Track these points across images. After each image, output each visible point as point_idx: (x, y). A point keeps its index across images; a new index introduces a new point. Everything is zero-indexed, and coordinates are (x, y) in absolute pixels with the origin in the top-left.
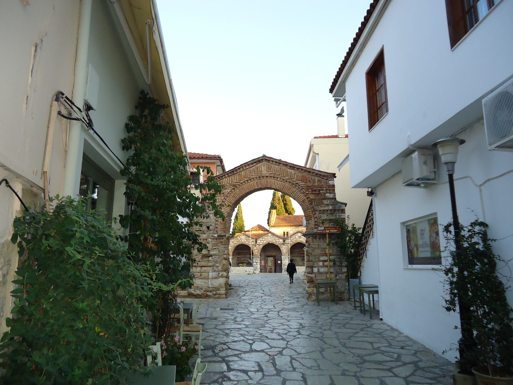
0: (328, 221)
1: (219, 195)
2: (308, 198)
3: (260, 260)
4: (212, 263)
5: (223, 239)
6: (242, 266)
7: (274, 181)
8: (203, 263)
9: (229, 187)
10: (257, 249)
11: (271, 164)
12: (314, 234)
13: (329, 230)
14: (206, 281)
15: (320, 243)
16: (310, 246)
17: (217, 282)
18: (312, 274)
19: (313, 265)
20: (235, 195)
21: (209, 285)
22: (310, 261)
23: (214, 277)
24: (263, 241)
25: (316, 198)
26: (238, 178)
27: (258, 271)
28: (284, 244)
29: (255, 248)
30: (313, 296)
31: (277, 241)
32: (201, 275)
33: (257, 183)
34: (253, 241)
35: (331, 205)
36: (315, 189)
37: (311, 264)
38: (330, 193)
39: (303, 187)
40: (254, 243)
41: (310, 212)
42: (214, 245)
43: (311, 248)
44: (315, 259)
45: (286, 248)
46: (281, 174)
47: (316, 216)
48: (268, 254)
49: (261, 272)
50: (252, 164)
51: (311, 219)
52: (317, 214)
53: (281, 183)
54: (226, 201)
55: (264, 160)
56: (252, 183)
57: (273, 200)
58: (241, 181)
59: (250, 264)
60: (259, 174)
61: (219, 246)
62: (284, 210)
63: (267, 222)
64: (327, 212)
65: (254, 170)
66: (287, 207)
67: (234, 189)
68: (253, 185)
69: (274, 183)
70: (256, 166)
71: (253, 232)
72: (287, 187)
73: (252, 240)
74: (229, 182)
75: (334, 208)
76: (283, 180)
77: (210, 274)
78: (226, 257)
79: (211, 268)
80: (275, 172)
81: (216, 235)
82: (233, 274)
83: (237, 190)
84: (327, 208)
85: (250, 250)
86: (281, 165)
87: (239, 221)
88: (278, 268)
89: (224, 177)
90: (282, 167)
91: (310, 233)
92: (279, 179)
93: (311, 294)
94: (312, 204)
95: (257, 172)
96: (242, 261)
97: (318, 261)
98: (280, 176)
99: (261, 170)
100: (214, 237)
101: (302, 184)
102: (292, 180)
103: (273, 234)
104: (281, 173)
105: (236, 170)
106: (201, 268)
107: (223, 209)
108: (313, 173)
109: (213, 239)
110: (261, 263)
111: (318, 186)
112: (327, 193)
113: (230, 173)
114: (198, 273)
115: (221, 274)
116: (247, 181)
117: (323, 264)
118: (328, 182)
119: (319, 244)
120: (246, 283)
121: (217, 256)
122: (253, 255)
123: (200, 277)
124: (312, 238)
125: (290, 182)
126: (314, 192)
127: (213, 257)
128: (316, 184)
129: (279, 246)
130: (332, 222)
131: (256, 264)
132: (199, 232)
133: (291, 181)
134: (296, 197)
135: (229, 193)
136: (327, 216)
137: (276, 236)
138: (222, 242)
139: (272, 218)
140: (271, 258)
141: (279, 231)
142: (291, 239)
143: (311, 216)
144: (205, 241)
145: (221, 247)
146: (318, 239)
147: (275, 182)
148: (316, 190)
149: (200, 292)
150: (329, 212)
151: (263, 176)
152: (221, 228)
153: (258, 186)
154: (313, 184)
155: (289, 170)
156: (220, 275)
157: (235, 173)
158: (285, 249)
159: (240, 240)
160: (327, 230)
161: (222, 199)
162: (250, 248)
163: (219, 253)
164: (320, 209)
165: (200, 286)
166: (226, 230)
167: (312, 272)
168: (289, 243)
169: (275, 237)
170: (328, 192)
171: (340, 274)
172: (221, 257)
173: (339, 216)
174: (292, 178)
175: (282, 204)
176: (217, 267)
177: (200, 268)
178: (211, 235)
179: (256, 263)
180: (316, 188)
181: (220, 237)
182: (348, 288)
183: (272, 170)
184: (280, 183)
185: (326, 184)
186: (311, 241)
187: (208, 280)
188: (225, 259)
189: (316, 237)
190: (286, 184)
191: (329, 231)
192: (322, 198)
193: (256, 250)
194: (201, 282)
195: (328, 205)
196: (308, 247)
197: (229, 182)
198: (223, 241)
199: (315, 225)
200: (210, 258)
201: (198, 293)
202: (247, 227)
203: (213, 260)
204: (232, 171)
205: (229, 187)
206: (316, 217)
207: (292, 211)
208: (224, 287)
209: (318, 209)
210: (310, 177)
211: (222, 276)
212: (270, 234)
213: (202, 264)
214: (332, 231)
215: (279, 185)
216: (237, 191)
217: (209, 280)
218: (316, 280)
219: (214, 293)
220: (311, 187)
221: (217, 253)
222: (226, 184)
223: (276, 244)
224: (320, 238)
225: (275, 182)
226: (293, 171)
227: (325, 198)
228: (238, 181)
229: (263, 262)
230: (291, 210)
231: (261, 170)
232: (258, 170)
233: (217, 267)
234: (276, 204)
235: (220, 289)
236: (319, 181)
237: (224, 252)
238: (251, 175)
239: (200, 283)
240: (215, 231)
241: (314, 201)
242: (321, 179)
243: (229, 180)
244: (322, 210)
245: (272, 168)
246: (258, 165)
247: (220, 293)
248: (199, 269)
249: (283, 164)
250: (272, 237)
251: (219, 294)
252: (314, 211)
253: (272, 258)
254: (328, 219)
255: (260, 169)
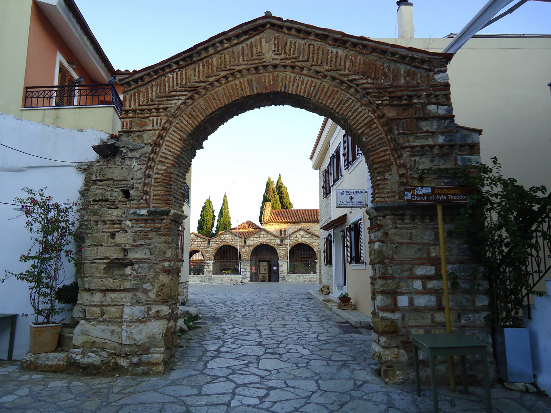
0: (435, 174)
1: (156, 114)
2: (379, 117)
3: (251, 266)
4: (133, 282)
5: (162, 220)
6: (226, 274)
7: (293, 75)
8: (111, 283)
9: (180, 93)
10: (246, 252)
11: (286, 36)
12: (399, 208)
13: (446, 195)
14: (114, 328)
15: (414, 232)
16: (386, 238)
17: (143, 332)
18: (392, 311)
19: (397, 288)
20: (195, 111)
21: (124, 338)
22: (389, 278)
23: (135, 318)
24: (253, 242)
25: (401, 117)
26: (203, 71)
27: (247, 281)
28: (281, 245)
29: (243, 250)
30: (398, 372)
31: (272, 241)
32: (103, 314)
33: (250, 83)
34: (240, 242)
35: (442, 133)
36: (399, 93)
37: (391, 284)
38: (438, 104)
39: (368, 88)
40: (243, 243)
41: (385, 151)
42: (138, 236)
43: (390, 245)
44: (402, 272)
45: (284, 250)
46: (311, 60)
47: (402, 161)
48: (261, 258)
49: (251, 281)
50: (238, 36)
51: (391, 170)
52: (405, 155)
53: (310, 80)
54: (173, 128)
55: (268, 26)
56: (237, 82)
57: (266, 192)
58: (211, 79)
59: (236, 271)
60: (256, 62)
61: (150, 239)
62: (280, 205)
63: (259, 219)
64: (432, 151)
65: (243, 51)
66: (284, 201)
67: (191, 98)
68: (239, 88)
69: (292, 81)
70: (249, 42)
71: (241, 230)
72: (325, 89)
73: (240, 240)
74: (179, 82)
75: (450, 140)
76: (317, 72)
77: (127, 310)
78: (169, 266)
79: (130, 295)
80: (296, 55)
81: (144, 212)
82: (214, 284)
83: (201, 100)
84: (430, 142)
85: (237, 253)
86: (310, 37)
87: (224, 218)
88: (273, 276)
89: (167, 70)
90: (313, 42)
91: (390, 204)
92: (305, 72)
93: (391, 367)
94: (391, 131)
95: (250, 56)
96: (226, 267)
97: (408, 278)
98: (309, 64)
99: (259, 50)
100: (139, 215)
101: (365, 81)
102: (340, 72)
103: (267, 232)
104: (311, 56)
105: (199, 53)
106: (105, 295)
107: (164, 146)
108: (394, 54)
109: (137, 220)
110: (251, 269)
111: (407, 87)
112: (430, 104)
113: (184, 60)
114: (94, 308)
115: (155, 309)
116: (225, 77)
117: (424, 287)
118: (433, 76)
119: (411, 233)
120: (227, 309)
121: (145, 265)
122: (240, 259)
123: (101, 319)
124: (392, 217)
125: (333, 79)
126: (395, 102)
127: (136, 266)
128: (402, 81)
129: (275, 247)
130: (447, 178)
131: (244, 270)
132: (103, 203)
133: (337, 76)
134: (350, 114)
135: (179, 108)
136: (432, 161)
137: (271, 234)
138: (160, 228)
139: (266, 212)
140: (264, 263)
141: (273, 228)
142: (291, 238)
143: (388, 163)
144: (115, 226)
145: (157, 242)
146: (408, 221)
147: (295, 78)
148: (403, 96)
149: (98, 358)
150: (436, 151)
151: (265, 64)
152: (159, 193)
153: (253, 90)
154: (393, 81)
155: (330, 49)
156: (152, 312)
157: (195, 59)
158: (283, 252)
159: (224, 239)
160: (440, 195)
161: (163, 122)
162: (237, 249)
163: (152, 256)
164: (412, 144)
165: (98, 340)
166: (171, 198)
167: (394, 308)
168: (288, 243)
169: (270, 236)
170: (433, 100)
171: (471, 311)
172: (157, 266)
173: (464, 160)
174: (338, 67)
175: (277, 197)
176: (146, 291)
177: (102, 294)
178: (131, 211)
179: (245, 269)
180: (401, 91)
181: (155, 215)
182: (492, 350)
183: (287, 50)
184: (308, 81)
185: (428, 81)
186: (391, 226)
187: (121, 326)
188: (167, 272)
189: (403, 215)
190: (324, 83)
191: (445, 198)
192: (417, 116)
193: (245, 253)
194: (103, 331)
195: (433, 133)
196: (383, 242)
197: (179, 82)
198: (163, 225)
199: (401, 184)
200: (128, 270)
201: (90, 360)
202: (234, 224)
203: (135, 273)
204: (188, 54)
205: (180, 93)
206: (403, 166)
207: (289, 206)
208: (162, 343)
209: (407, 144)
210: (386, 65)
211: (158, 316)
212: (263, 233)
213: (105, 285)
214: (454, 197)
215: (306, 86)
216: (200, 101)
217: (124, 327)
218: (404, 327)
219: (135, 360)
220: (389, 90)
221: (146, 257)
222: (173, 87)
223: (271, 245)
224: (413, 218)
225: (295, 78)
226: (341, 52)
227: (426, 116)
228: (202, 79)
229: (254, 268)
230: (288, 204)
231: (259, 50)
232: (252, 51)
233: (146, 291)
234: (270, 198)
235: (151, 350)
236: (408, 73)
237: (165, 253)
238: (236, 63)
239: (100, 335)
240: (141, 201)
241: (397, 125)
242: (415, 69)
243: (179, 77)
244: (416, 146)
245: (288, 44)
246: (253, 40)
247: (151, 360)
248: (98, 297)
249: (317, 35)
250: (266, 236)
251: (148, 363)
252: (398, 149)
253: (265, 264)
254: (434, 168)
255: (259, 47)
